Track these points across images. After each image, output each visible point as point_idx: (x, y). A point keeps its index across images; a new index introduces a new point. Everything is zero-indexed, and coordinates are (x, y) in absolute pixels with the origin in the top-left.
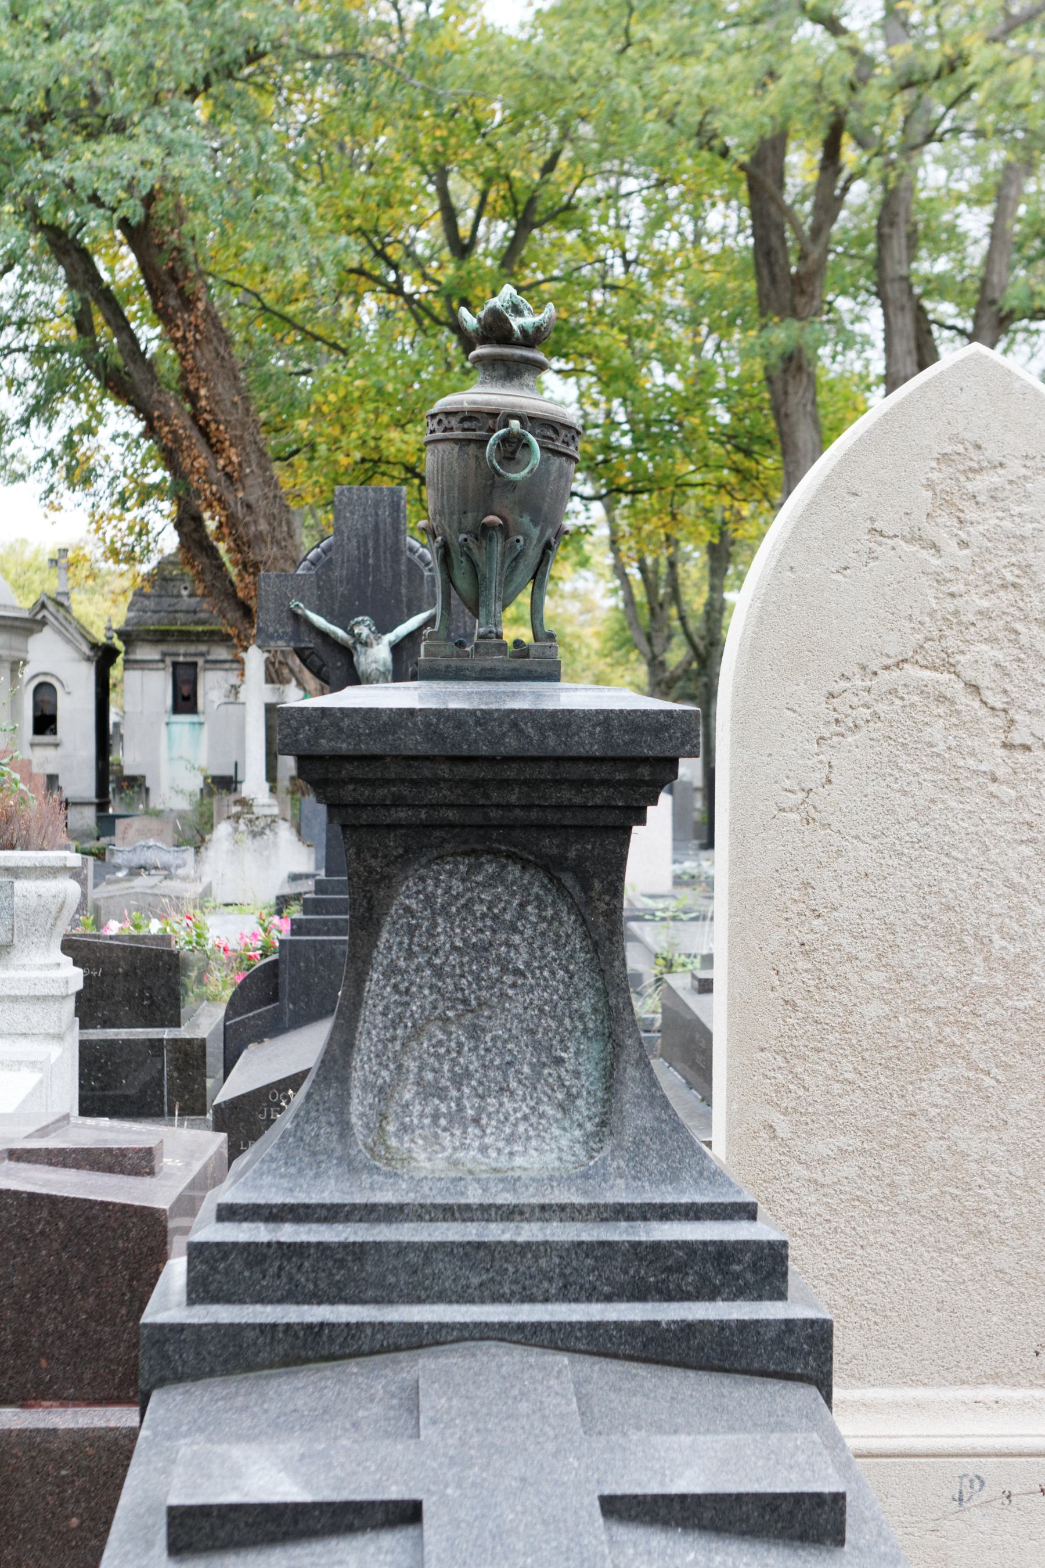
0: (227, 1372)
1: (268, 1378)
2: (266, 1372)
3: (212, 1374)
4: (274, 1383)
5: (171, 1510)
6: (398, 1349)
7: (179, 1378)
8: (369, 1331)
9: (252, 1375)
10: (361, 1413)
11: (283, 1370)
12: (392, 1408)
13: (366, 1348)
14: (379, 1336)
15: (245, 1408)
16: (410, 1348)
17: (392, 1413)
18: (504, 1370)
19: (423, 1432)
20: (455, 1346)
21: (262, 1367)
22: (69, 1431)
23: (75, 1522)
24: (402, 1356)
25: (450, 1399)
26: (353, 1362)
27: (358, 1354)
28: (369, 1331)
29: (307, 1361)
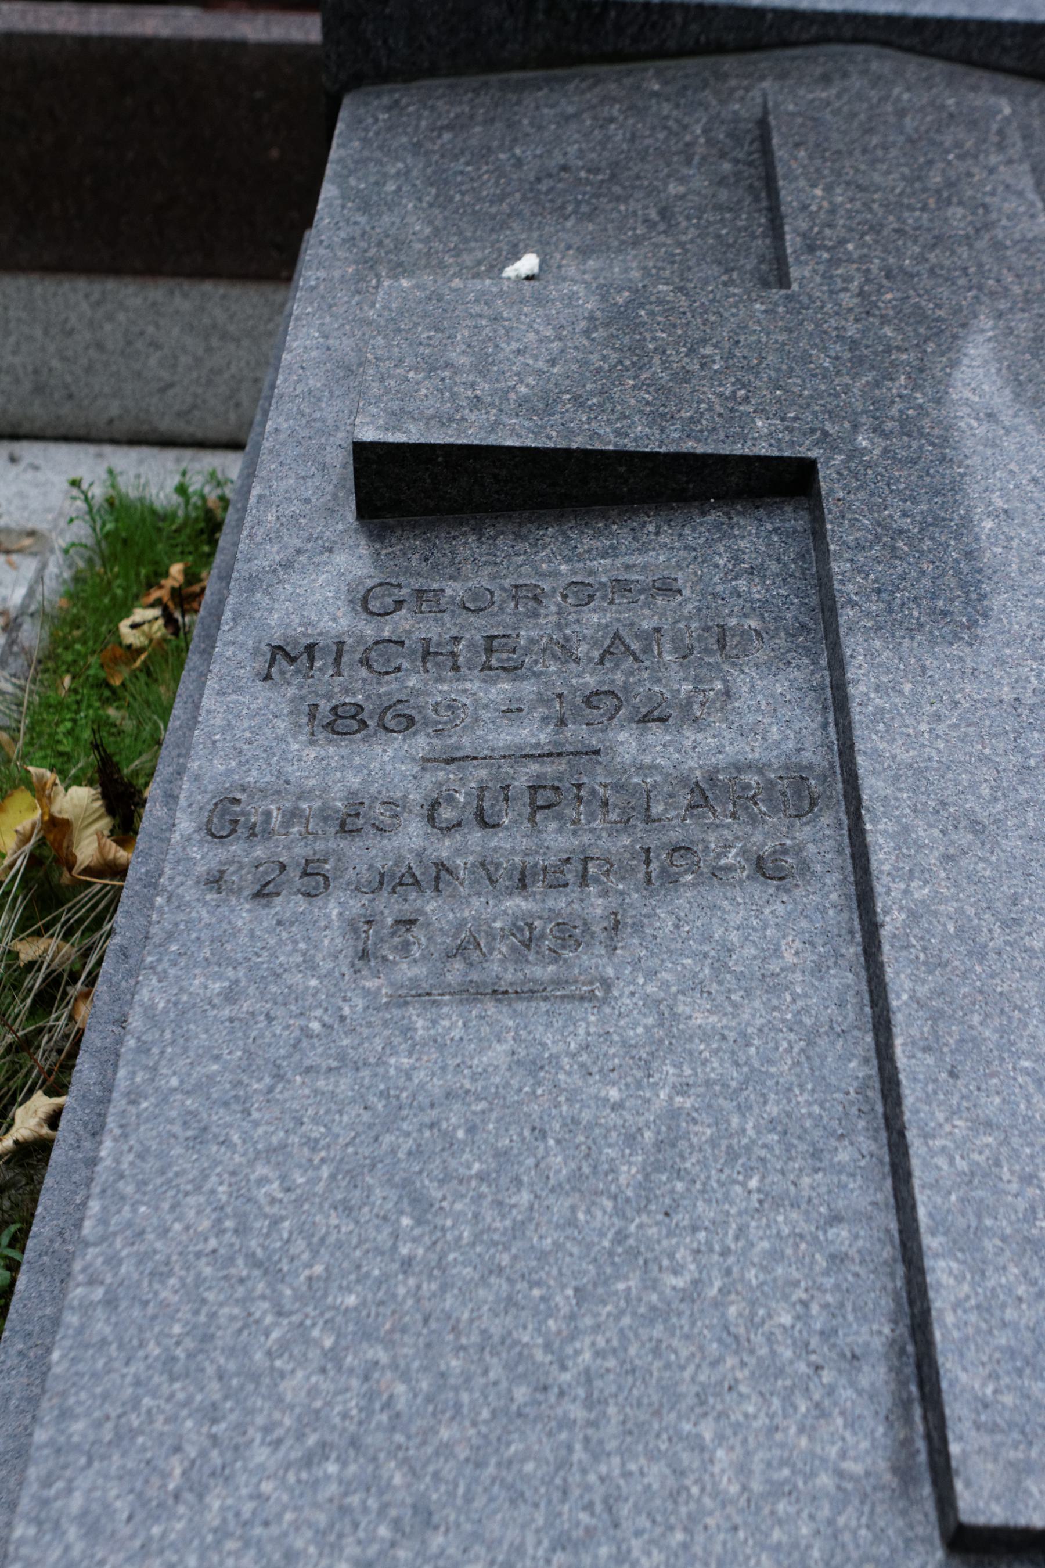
0: (456, 71)
1: (521, 87)
2: (516, 75)
3: (432, 72)
4: (529, 100)
5: (361, 450)
6: (720, 49)
7: (383, 76)
8: (679, 19)
9: (494, 78)
10: (674, 188)
11: (540, 74)
12: (722, 182)
13: (671, 44)
14: (694, 27)
15: (485, 153)
16: (742, 48)
17: (724, 195)
18: (909, 122)
19: (794, 272)
20: (812, 51)
21: (509, 66)
22: (261, 46)
23: (275, 153)
24: (729, 63)
25: (829, 189)
26: (651, 68)
27: (661, 54)
28: (679, 19)
29: (580, 60)
